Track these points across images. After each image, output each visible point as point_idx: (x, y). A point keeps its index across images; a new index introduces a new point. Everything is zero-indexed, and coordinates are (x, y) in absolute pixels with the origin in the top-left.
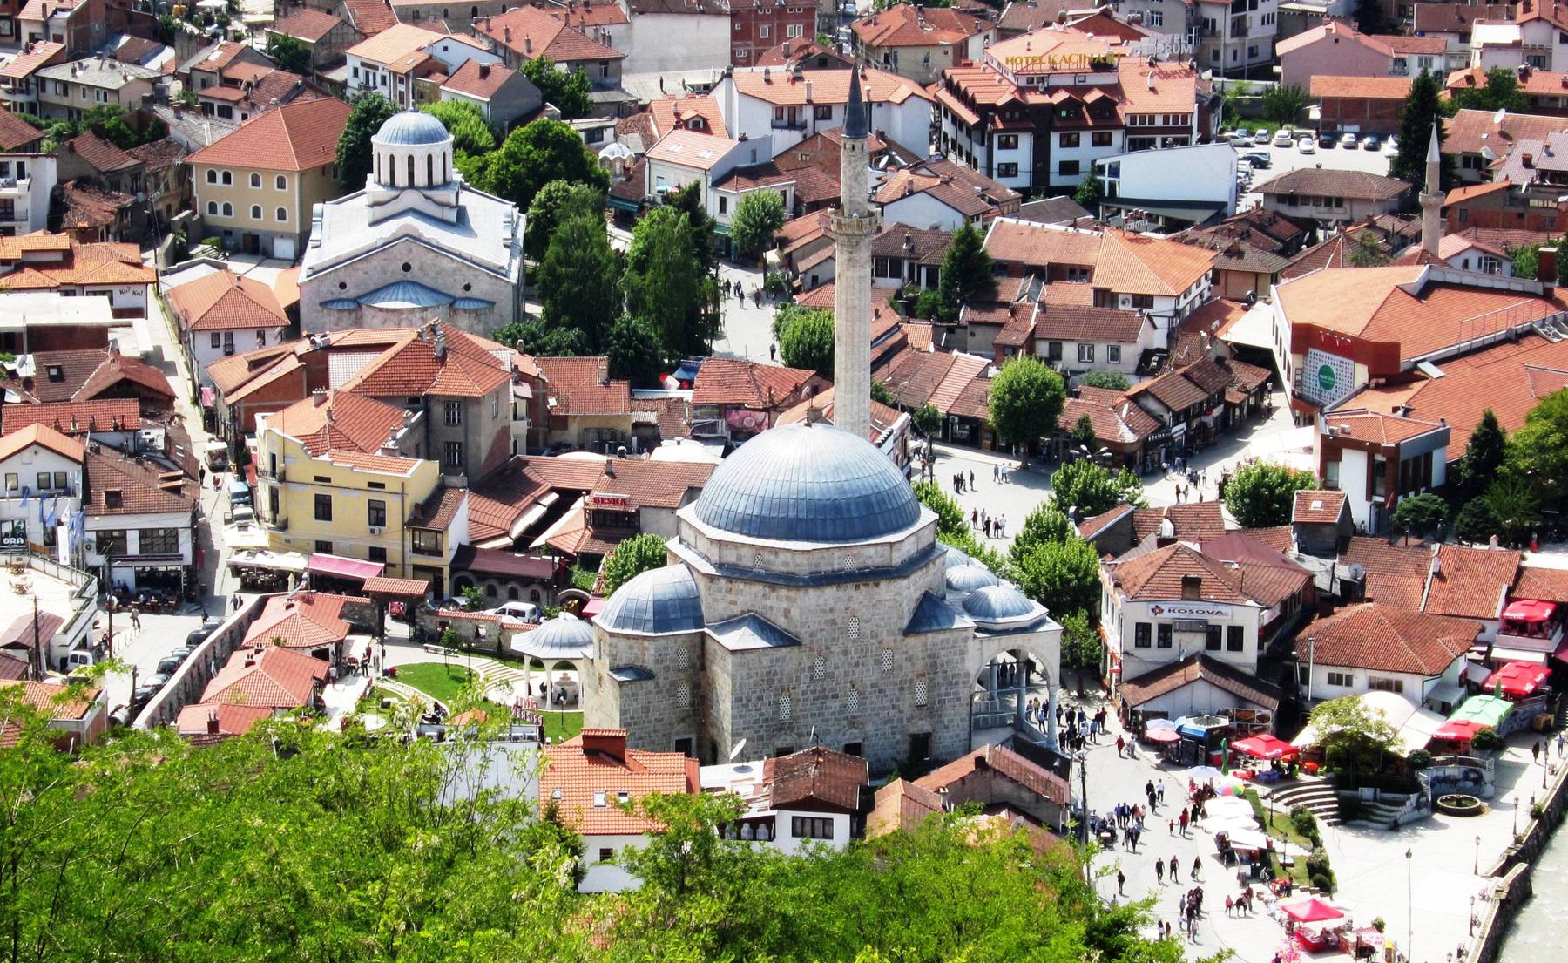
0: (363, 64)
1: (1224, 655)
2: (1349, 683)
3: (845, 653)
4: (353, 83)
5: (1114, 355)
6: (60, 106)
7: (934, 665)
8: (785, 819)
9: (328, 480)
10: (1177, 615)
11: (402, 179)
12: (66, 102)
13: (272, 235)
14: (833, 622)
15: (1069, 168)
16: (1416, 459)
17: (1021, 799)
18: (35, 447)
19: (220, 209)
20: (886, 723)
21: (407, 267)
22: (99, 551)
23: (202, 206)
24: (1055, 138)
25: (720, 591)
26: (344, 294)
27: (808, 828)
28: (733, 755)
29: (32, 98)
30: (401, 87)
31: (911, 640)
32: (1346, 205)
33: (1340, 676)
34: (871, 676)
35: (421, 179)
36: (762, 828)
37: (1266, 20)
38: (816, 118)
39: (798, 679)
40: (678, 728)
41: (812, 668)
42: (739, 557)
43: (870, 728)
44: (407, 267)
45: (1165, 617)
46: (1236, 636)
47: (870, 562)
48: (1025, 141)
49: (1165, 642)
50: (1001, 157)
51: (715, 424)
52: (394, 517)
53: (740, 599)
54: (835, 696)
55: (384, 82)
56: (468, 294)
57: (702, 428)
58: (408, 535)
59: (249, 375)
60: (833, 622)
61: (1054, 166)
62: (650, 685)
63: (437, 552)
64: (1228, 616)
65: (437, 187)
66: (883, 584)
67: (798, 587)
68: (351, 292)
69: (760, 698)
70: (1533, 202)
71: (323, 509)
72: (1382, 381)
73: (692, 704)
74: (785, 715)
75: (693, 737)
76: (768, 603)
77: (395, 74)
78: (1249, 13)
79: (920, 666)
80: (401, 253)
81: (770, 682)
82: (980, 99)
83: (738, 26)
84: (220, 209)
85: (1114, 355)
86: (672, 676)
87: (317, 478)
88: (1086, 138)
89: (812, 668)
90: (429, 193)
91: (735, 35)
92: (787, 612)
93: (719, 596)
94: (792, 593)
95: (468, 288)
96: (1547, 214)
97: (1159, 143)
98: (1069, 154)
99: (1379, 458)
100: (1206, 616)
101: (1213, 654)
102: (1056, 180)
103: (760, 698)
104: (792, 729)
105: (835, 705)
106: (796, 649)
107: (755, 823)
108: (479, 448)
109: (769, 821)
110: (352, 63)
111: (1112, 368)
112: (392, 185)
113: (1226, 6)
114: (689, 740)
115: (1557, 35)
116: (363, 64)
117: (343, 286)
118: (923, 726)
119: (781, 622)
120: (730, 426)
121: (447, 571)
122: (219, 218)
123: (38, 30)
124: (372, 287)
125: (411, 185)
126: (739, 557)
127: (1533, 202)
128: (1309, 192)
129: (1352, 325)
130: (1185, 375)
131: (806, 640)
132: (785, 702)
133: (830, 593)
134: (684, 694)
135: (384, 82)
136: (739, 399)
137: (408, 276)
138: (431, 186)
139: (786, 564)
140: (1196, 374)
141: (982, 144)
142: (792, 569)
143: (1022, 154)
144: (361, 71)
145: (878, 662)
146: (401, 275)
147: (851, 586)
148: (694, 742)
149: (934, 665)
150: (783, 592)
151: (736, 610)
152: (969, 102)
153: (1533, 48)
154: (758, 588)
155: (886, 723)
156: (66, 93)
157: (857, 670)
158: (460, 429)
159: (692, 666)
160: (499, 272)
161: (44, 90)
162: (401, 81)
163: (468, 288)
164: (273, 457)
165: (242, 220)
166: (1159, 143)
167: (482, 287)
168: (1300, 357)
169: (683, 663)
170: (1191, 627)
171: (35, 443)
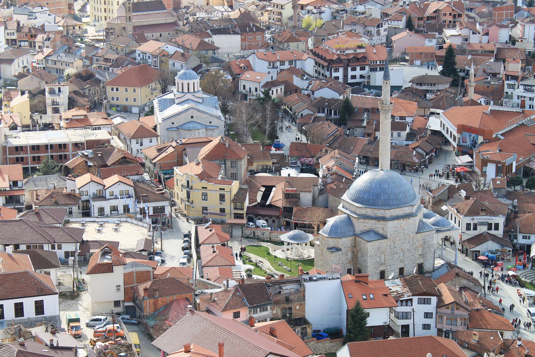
0: (142, 53)
1: (493, 232)
2: (529, 238)
3: (400, 240)
4: (138, 58)
5: (399, 135)
6: (53, 68)
7: (424, 242)
8: (415, 299)
9: (206, 188)
10: (479, 220)
11: (186, 90)
12: (55, 66)
13: (131, 107)
14: (397, 231)
15: (354, 77)
16: (509, 165)
17: (470, 285)
18: (119, 183)
19: (115, 99)
20: (411, 260)
21: (192, 117)
22: (141, 214)
23: (110, 98)
24: (349, 69)
25: (361, 222)
26: (173, 126)
27: (423, 302)
28: (390, 277)
29: (44, 66)
30: (155, 59)
31: (418, 235)
32: (436, 85)
33: (526, 236)
34: (407, 246)
35: (191, 90)
36: (409, 302)
37: (385, 30)
38: (280, 65)
39: (387, 249)
40: (348, 265)
41: (390, 245)
42: (367, 212)
43: (406, 262)
44: (192, 117)
45: (476, 221)
46: (497, 227)
47: (406, 212)
48: (341, 70)
49: (475, 229)
50: (334, 74)
51: (296, 162)
52: (227, 198)
53: (367, 225)
54: (397, 253)
55: (149, 58)
56: (211, 124)
57: (292, 163)
58: (232, 204)
59: (158, 154)
60: (397, 231)
61: (349, 77)
62: (340, 252)
63: (243, 209)
64: (494, 220)
65: (196, 92)
66: (411, 218)
67: (387, 221)
68: (176, 125)
69: (376, 255)
70: (492, 83)
71: (205, 197)
72: (488, 141)
73: (352, 258)
74: (382, 261)
75: (352, 268)
76: (377, 226)
77: (153, 55)
78: (381, 28)
79: (420, 243)
80: (190, 113)
81: (379, 250)
82: (327, 58)
83: (243, 37)
84: (115, 99)
85: (399, 135)
86: (347, 249)
87: (203, 188)
88: (358, 68)
89: (390, 245)
90: (194, 94)
91: (242, 40)
92: (383, 229)
93: (360, 224)
94: (385, 223)
95: (210, 122)
96: (495, 86)
97: (378, 69)
98: (353, 73)
99: (499, 165)
100: (487, 221)
101: (490, 232)
102: (350, 81)
103: (376, 255)
104: (384, 264)
105: (396, 256)
106: (386, 240)
107: (407, 301)
108: (241, 174)
109: (411, 300)
110: (137, 52)
111: (399, 139)
112: (183, 92)
113: (375, 27)
114: (351, 269)
115: (471, 32)
116: (142, 53)
117: (173, 123)
118: (421, 261)
119: (381, 232)
120: (301, 162)
121: (245, 215)
122: (115, 102)
123: (41, 44)
124: (182, 124)
125: (189, 92)
126: (367, 212)
127: (492, 83)
128: (426, 82)
129: (476, 124)
130: (426, 141)
131: (389, 236)
132: (383, 256)
133: (396, 222)
134: (350, 255)
135: (149, 58)
136: (303, 154)
137: (193, 120)
138: (194, 92)
139: (382, 214)
140: (429, 141)
141: (328, 71)
142: (384, 215)
143: (340, 74)
144: (141, 55)
145: (409, 242)
146: (191, 120)
147: (402, 220)
148: (352, 270)
149: (424, 242)
150: (382, 222)
151: (366, 228)
152: (325, 59)
153: (465, 36)
154: (373, 222)
155: (411, 260)
156: (55, 64)
157: (403, 245)
158: (235, 169)
159: (352, 246)
160: (219, 118)
161: (48, 63)
162: (155, 57)
163: (210, 122)
164: (188, 182)
165: (122, 102)
166: (378, 69)
167: (215, 122)
168: (459, 135)
169: (350, 246)
170: (482, 224)
171: (119, 181)
